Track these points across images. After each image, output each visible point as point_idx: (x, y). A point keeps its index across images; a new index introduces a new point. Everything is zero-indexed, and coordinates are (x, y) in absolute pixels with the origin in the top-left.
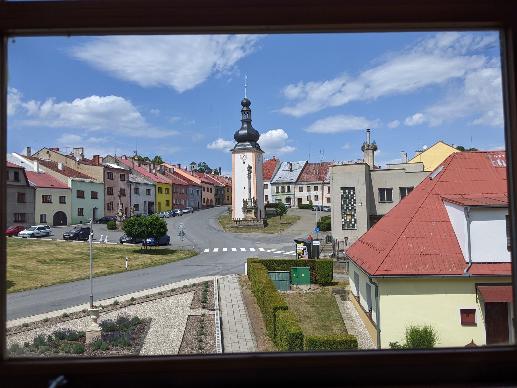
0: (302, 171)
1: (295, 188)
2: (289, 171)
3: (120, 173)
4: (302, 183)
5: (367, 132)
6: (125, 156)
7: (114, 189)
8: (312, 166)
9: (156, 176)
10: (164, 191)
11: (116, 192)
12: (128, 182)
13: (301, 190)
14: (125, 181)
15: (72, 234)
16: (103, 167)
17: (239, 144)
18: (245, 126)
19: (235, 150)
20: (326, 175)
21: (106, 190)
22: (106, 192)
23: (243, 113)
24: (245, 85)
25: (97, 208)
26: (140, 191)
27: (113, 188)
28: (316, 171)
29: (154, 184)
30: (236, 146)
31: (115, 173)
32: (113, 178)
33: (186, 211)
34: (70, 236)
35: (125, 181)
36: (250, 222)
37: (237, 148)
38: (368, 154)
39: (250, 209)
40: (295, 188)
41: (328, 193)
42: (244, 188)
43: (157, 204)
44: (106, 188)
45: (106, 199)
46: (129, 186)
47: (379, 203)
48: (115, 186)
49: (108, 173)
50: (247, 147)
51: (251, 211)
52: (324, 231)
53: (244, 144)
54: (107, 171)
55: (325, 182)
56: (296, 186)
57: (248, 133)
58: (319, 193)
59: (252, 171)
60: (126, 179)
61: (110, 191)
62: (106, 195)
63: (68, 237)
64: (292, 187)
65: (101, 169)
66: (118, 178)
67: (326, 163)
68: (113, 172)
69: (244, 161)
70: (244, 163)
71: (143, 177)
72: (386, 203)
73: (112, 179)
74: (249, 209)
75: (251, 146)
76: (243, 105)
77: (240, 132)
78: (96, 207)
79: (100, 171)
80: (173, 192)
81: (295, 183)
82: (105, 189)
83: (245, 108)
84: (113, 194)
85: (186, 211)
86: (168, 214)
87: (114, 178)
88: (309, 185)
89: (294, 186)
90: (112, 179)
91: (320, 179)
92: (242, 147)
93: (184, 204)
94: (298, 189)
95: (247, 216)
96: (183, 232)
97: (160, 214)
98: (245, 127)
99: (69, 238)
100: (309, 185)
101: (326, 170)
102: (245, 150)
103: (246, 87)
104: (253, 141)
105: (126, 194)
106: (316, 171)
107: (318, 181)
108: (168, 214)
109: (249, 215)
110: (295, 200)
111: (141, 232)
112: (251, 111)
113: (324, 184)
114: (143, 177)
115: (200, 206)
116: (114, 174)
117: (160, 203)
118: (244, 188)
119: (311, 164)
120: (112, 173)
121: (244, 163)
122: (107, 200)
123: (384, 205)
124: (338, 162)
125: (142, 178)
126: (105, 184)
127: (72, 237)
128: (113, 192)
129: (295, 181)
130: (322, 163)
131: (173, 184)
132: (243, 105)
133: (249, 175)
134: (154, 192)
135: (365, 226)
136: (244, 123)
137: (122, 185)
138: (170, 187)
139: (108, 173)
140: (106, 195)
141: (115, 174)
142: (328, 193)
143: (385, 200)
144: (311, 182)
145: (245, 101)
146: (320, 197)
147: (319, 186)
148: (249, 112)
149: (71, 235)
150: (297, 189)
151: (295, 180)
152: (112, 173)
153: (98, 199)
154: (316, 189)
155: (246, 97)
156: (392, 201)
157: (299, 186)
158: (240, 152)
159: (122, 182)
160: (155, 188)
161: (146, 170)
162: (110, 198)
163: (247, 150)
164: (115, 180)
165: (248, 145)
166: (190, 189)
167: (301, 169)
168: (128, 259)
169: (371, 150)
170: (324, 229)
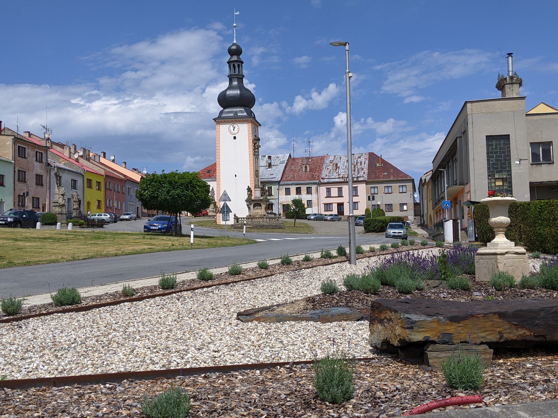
0: (286, 167)
1: (278, 189)
2: (268, 167)
3: (36, 150)
4: (289, 182)
5: (508, 57)
6: (29, 132)
7: (27, 173)
8: (297, 161)
9: (79, 162)
10: (94, 184)
11: (31, 179)
12: (47, 164)
13: (288, 192)
14: (42, 162)
15: (10, 218)
16: (13, 137)
17: (226, 110)
18: (235, 83)
19: (220, 120)
20: (321, 173)
21: (17, 173)
22: (17, 178)
23: (232, 65)
24: (235, 25)
25: (3, 201)
26: (63, 181)
27: (25, 172)
28: (306, 167)
29: (82, 172)
30: (221, 113)
31: (28, 149)
32: (26, 156)
33: (127, 217)
34: (7, 220)
35: (42, 162)
36: (261, 220)
37: (224, 115)
38: (513, 90)
39: (259, 202)
40: (278, 189)
41: (326, 197)
42: (236, 175)
43: (86, 203)
44: (16, 170)
45: (16, 189)
46: (49, 171)
47: (531, 164)
48: (29, 170)
49: (19, 147)
50: (239, 114)
51: (260, 205)
52: (377, 232)
53: (235, 110)
54: (18, 145)
55: (322, 181)
56: (280, 187)
57: (241, 94)
58: (313, 197)
59: (260, 145)
60: (44, 161)
61: (21, 177)
62: (17, 182)
63: (4, 223)
64: (274, 188)
65: (9, 140)
66: (33, 157)
67: (316, 157)
68: (27, 147)
69: (235, 136)
70: (235, 138)
71: (64, 162)
72: (543, 165)
73: (25, 158)
74: (257, 202)
75: (245, 114)
76: (231, 52)
77: (228, 92)
78: (1, 200)
79: (7, 143)
80: (106, 189)
81: (278, 183)
82: (15, 172)
83: (235, 58)
84: (26, 181)
85: (127, 217)
86: (109, 216)
87: (28, 156)
88: (299, 186)
89: (277, 187)
90: (25, 158)
91: (313, 178)
92: (232, 115)
93: (119, 208)
94: (283, 191)
95: (254, 212)
96: (227, 206)
97: (96, 216)
98: (236, 85)
99: (5, 224)
100: (299, 186)
101: (320, 167)
102: (236, 120)
103: (235, 27)
104: (248, 107)
105: (44, 183)
106: (306, 167)
107: (312, 180)
108: (109, 216)
109: (257, 211)
110: (280, 207)
111: (176, 196)
112: (242, 63)
113: (320, 184)
114: (64, 162)
115: (140, 214)
116: (27, 150)
117: (89, 203)
118: (236, 175)
119: (296, 158)
120: (25, 148)
121: (235, 138)
122: (18, 189)
123: (539, 167)
124: (333, 156)
125: (61, 163)
126: (14, 164)
127: (10, 222)
128: (26, 179)
129: (279, 179)
130: (312, 157)
131: (106, 176)
132: (231, 52)
133: (256, 150)
134: (82, 185)
135: (526, 196)
136: (233, 79)
137: (38, 169)
138: (102, 180)
139: (19, 147)
140: (17, 182)
141: (30, 151)
142: (326, 197)
143: (540, 161)
144: (301, 182)
145: (234, 47)
146: (315, 201)
147: (314, 187)
148: (240, 64)
149: (9, 220)
150: (282, 191)
151: (278, 178)
152: (25, 148)
153: (5, 186)
154: (309, 191)
155: (235, 42)
156: (550, 162)
157: (284, 187)
158: (228, 122)
159: (38, 164)
160: (83, 178)
161: (63, 154)
162: (22, 188)
163: (240, 119)
164: (29, 159)
165: (241, 112)
166: (127, 186)
167: (284, 165)
168: (195, 226)
169: (516, 83)
170: (377, 229)
